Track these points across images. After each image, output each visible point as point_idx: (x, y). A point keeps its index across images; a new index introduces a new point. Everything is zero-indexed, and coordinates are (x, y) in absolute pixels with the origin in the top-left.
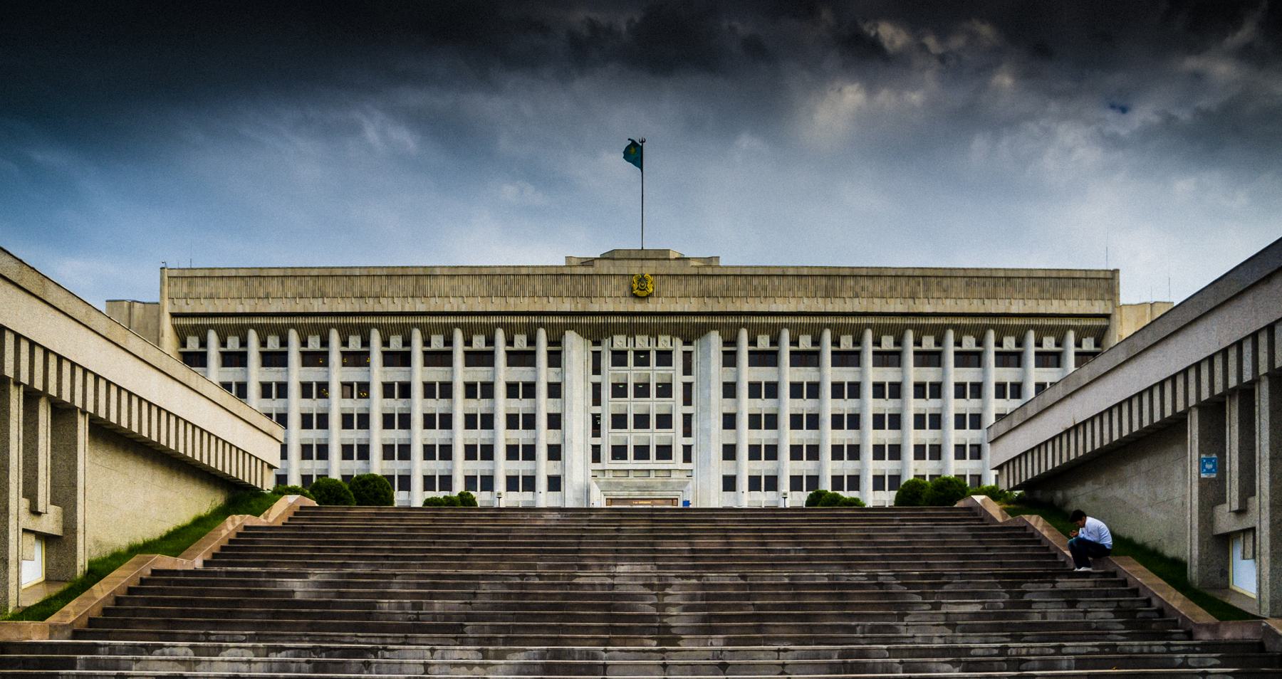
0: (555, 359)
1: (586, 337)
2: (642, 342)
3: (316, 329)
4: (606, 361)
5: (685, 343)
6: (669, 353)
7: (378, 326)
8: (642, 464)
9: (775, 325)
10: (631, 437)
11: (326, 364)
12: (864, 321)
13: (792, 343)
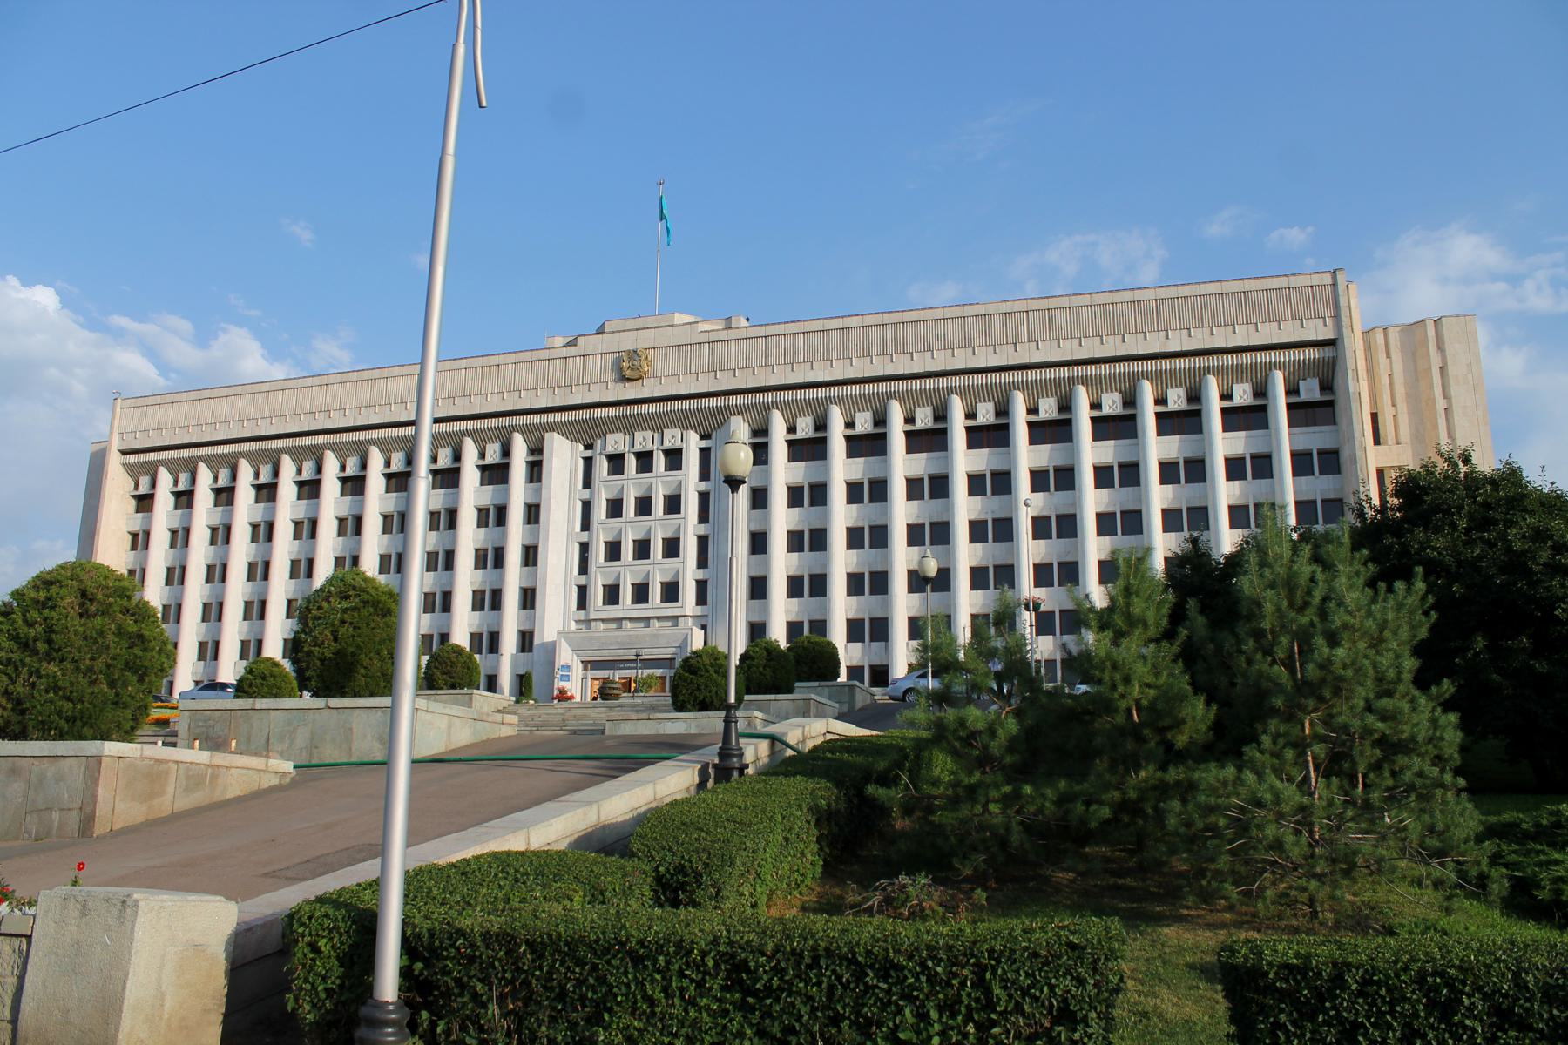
0: (535, 470)
1: (575, 439)
2: (644, 440)
3: (1241, 373)
4: (602, 466)
5: (702, 437)
6: (679, 452)
7: (473, 434)
8: (641, 611)
9: (150, 463)
10: (628, 572)
11: (1264, 425)
12: (771, 397)
13: (1223, 397)
